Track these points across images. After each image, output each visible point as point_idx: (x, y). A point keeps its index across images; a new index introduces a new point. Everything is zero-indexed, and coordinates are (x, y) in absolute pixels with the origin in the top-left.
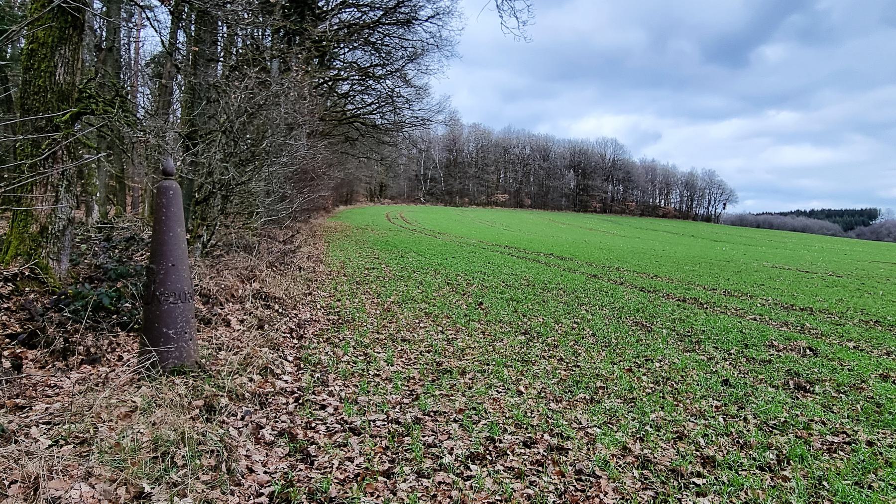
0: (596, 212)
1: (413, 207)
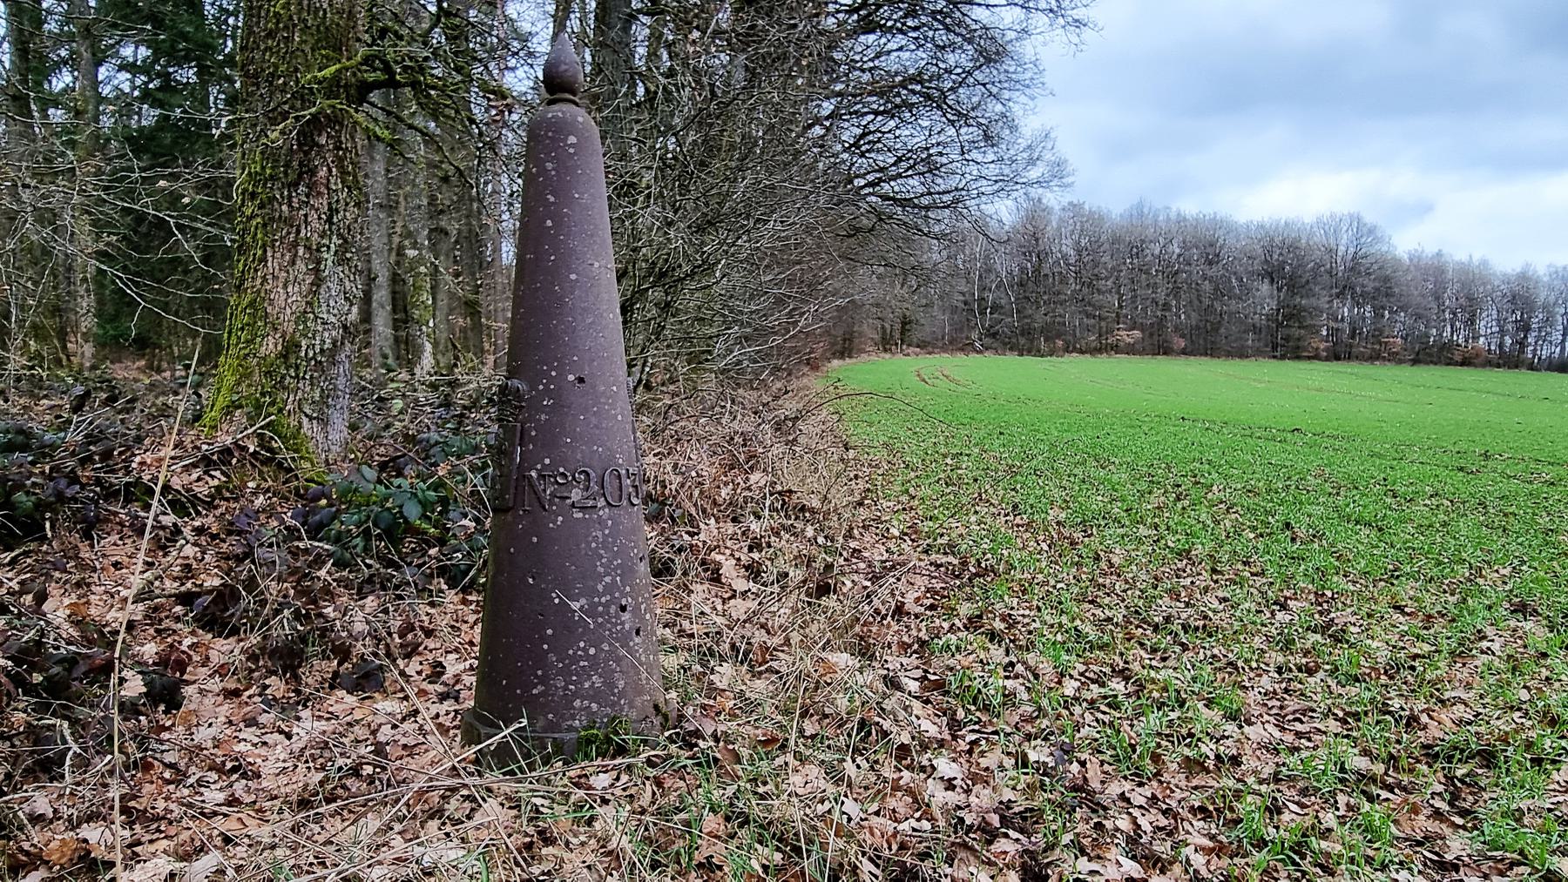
0: (1316, 357)
1: (960, 358)
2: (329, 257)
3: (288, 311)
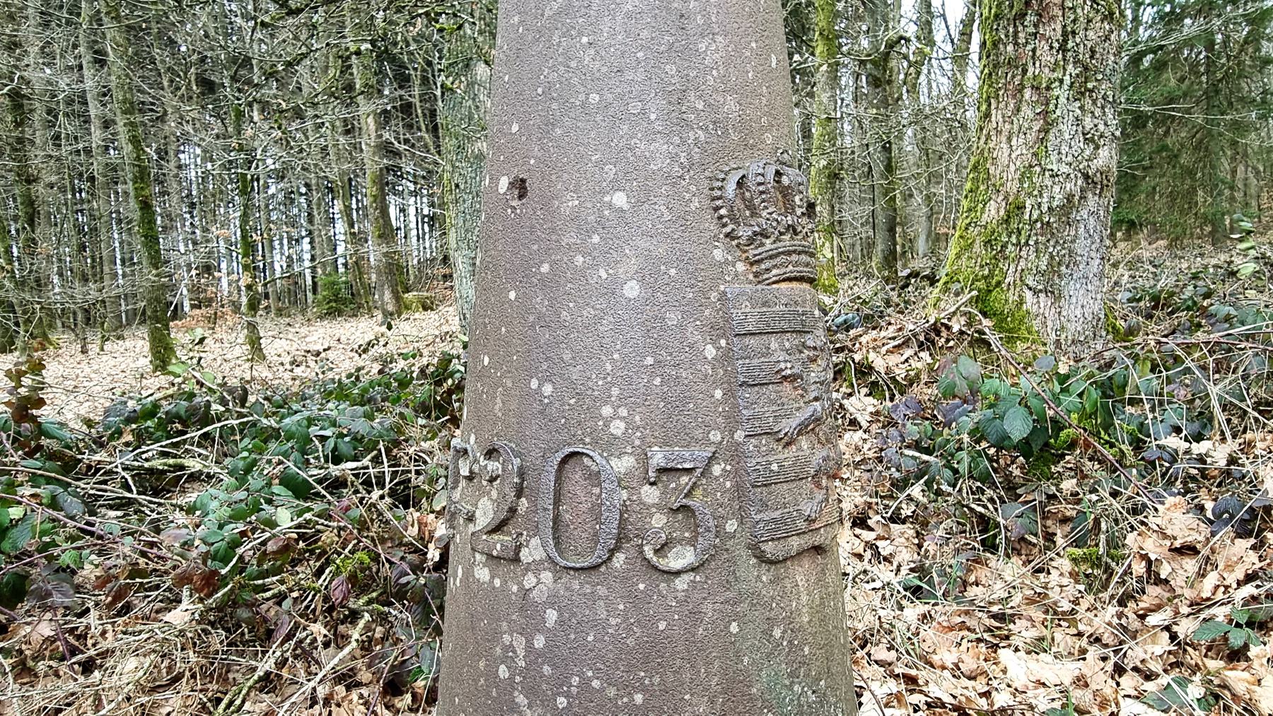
2: (1062, 93)
3: (1012, 168)
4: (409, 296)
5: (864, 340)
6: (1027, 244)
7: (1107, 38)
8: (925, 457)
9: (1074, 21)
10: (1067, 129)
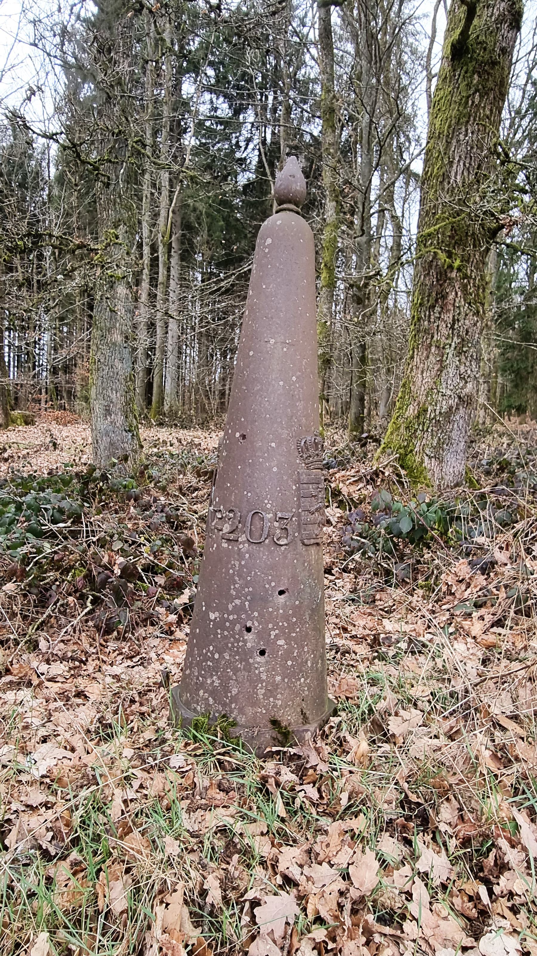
2: (450, 351)
3: (423, 389)
4: (16, 413)
5: (337, 476)
6: (427, 431)
7: (475, 325)
8: (363, 540)
9: (459, 314)
10: (451, 371)
